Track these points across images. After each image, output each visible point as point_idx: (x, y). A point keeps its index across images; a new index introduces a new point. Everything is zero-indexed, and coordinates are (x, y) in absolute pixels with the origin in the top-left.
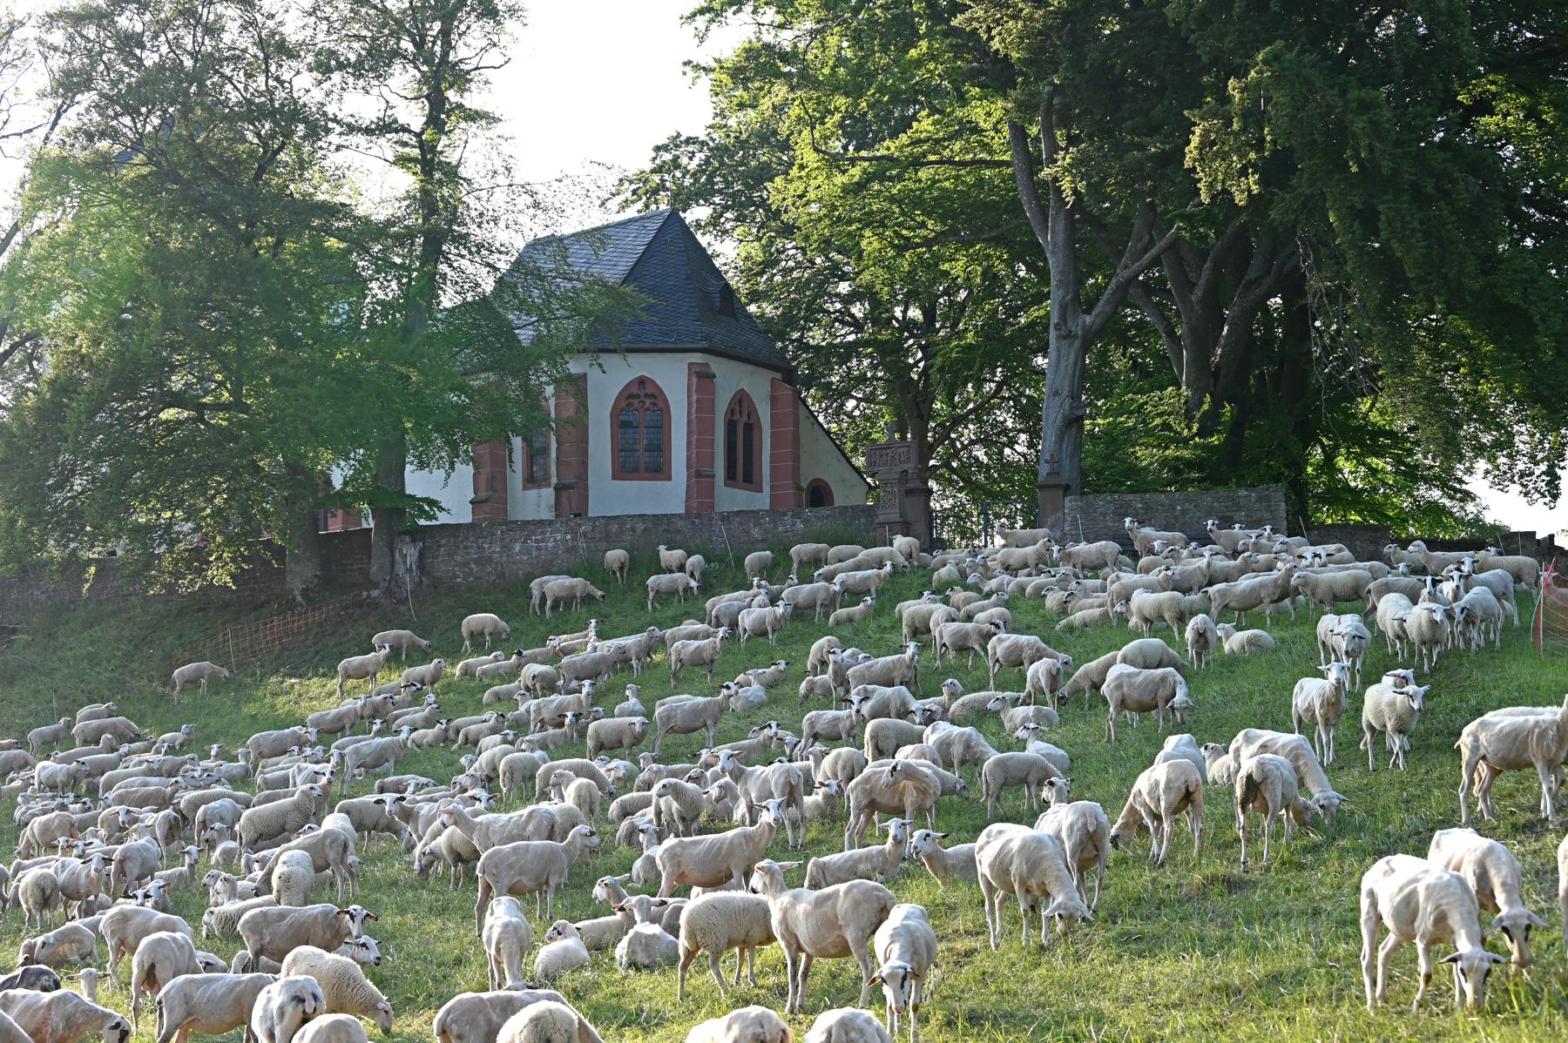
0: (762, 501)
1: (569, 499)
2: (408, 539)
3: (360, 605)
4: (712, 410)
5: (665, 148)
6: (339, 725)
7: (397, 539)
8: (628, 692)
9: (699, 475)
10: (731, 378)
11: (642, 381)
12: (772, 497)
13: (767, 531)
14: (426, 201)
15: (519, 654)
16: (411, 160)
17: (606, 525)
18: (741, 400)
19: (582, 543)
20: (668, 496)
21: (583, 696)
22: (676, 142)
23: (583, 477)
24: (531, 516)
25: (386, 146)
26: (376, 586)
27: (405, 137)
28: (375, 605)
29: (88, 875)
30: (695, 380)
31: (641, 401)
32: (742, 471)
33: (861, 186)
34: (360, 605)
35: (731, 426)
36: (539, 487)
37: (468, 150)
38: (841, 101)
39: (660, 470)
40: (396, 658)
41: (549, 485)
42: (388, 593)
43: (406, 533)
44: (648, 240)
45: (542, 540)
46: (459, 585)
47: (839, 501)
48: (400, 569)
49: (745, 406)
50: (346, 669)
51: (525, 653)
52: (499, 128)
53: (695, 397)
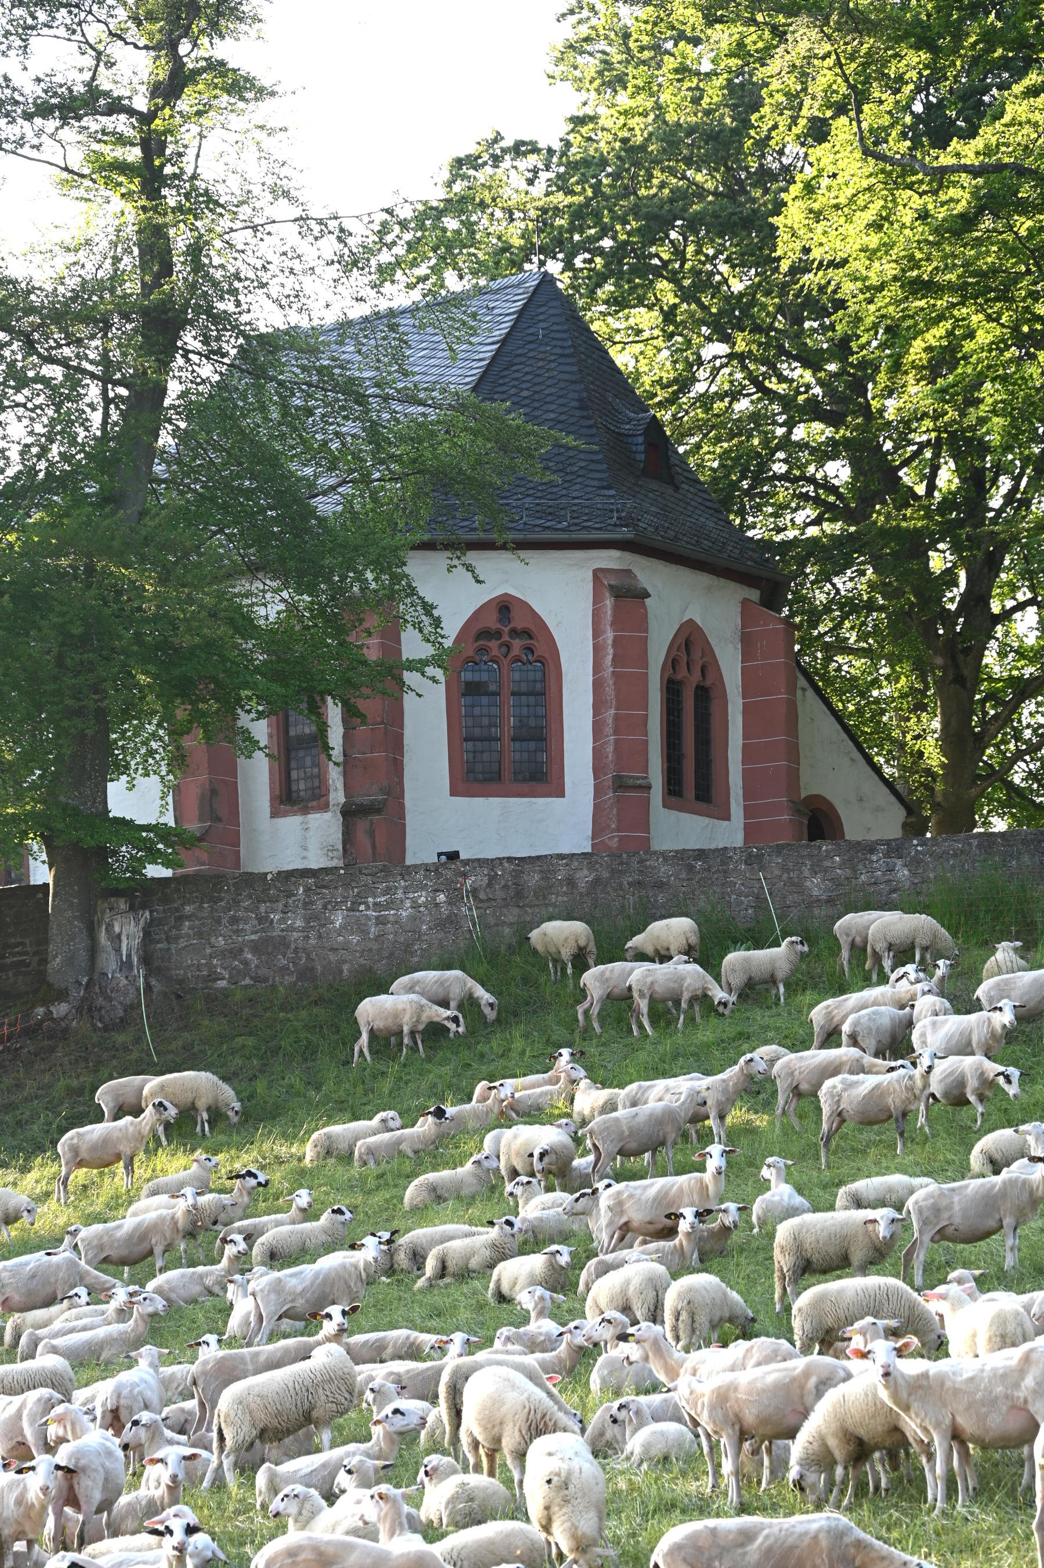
0: (729, 833)
1: (371, 834)
2: (123, 904)
3: (31, 1032)
4: (643, 660)
5: (472, 161)
6: (143, 1248)
7: (102, 905)
8: (765, 1172)
9: (618, 786)
10: (680, 600)
11: (505, 606)
12: (748, 829)
13: (837, 882)
14: (153, 246)
15: (440, 1113)
16: (122, 167)
17: (517, 874)
18: (690, 641)
19: (468, 910)
20: (562, 823)
21: (708, 1177)
22: (498, 151)
23: (395, 791)
24: (292, 862)
25: (71, 144)
26: (62, 995)
27: (121, 123)
28: (60, 1033)
29: (20, 1501)
30: (609, 602)
31: (509, 635)
32: (694, 782)
33: (967, 221)
34: (31, 1032)
35: (672, 690)
36: (305, 811)
37: (214, 150)
38: (912, 61)
39: (540, 776)
40: (183, 1127)
41: (325, 807)
42: (86, 1008)
43: (117, 893)
44: (500, 332)
45: (388, 906)
46: (226, 993)
47: (852, 832)
48: (109, 964)
49: (697, 654)
50: (75, 1150)
51: (450, 1111)
52: (262, 111)
53: (609, 635)
